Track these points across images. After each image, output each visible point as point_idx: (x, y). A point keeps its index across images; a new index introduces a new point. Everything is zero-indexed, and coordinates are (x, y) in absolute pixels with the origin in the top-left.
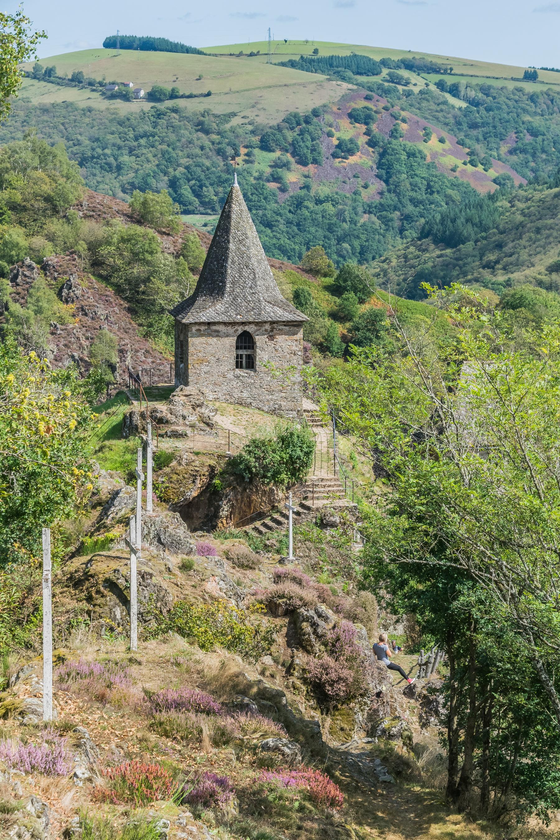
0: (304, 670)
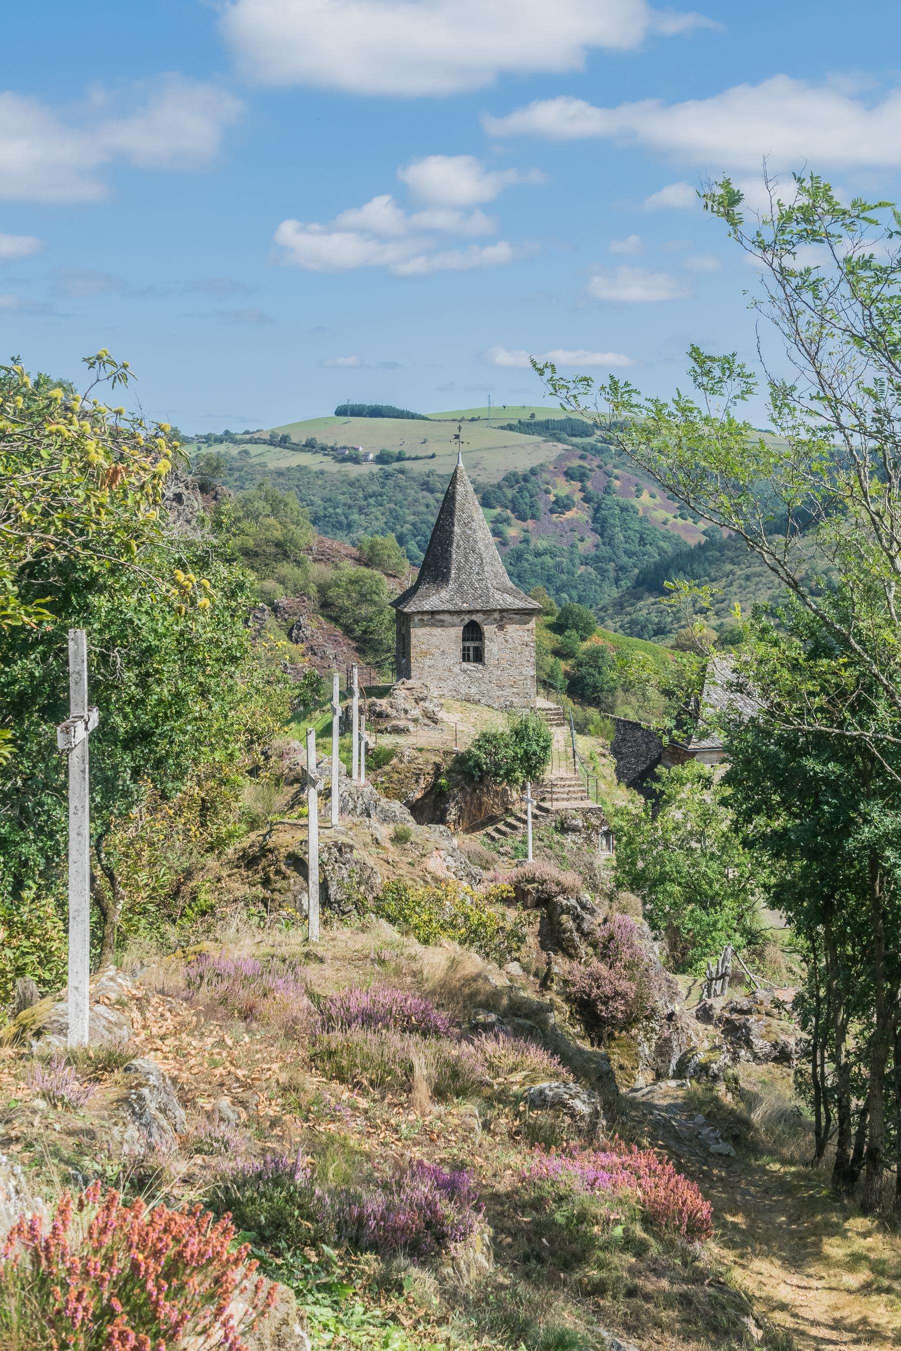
0: (566, 982)
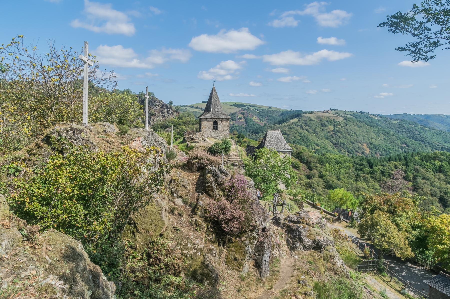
0: (205, 210)
